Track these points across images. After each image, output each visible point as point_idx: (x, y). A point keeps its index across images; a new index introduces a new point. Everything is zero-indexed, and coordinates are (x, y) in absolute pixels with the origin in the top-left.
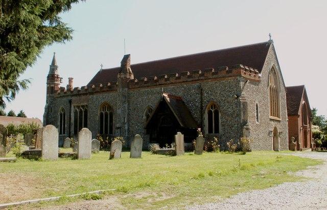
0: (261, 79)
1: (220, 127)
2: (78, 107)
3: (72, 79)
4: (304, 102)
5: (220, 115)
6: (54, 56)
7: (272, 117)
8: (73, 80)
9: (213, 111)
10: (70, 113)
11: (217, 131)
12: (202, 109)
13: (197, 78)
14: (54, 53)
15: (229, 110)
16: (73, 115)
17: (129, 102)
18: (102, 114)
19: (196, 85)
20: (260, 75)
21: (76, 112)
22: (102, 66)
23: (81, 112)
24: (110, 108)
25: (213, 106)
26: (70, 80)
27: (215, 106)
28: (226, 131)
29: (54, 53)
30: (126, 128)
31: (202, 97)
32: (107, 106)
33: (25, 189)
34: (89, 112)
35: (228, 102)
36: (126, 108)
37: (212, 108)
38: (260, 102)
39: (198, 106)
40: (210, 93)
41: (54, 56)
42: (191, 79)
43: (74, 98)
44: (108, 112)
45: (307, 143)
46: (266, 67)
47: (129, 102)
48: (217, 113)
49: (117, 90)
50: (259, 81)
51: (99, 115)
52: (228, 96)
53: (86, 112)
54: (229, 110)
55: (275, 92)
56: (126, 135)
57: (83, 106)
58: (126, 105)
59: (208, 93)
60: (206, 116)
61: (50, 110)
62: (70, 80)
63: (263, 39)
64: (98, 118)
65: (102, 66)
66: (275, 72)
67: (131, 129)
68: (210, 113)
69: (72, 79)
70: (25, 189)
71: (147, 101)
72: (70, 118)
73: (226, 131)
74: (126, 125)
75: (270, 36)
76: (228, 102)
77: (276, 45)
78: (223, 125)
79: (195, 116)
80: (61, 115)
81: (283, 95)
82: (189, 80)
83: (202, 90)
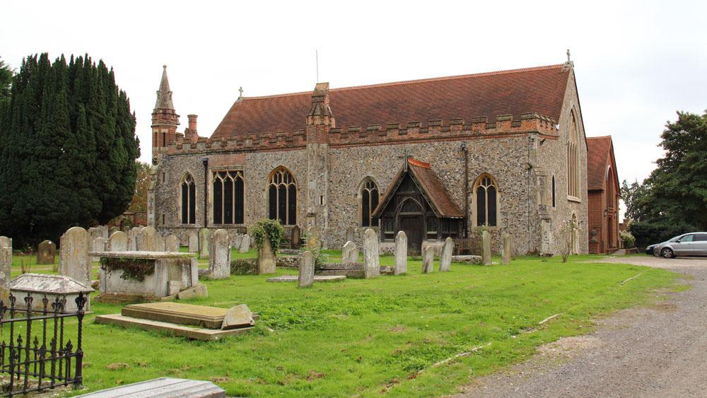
0: (559, 133)
1: (499, 217)
2: (223, 174)
3: (195, 116)
4: (609, 166)
5: (498, 196)
6: (165, 73)
7: (570, 198)
8: (198, 120)
9: (486, 188)
10: (206, 183)
11: (493, 222)
12: (467, 185)
13: (458, 133)
14: (165, 67)
15: (515, 188)
16: (211, 188)
17: (330, 169)
18: (272, 189)
19: (457, 144)
20: (558, 127)
21: (217, 184)
22: (241, 90)
23: (228, 182)
24: (289, 177)
25: (486, 179)
26: (192, 119)
27: (489, 180)
28: (510, 223)
29: (165, 67)
30: (326, 215)
31: (467, 167)
32: (281, 174)
33: (587, 339)
34: (247, 185)
35: (513, 175)
36: (326, 180)
37: (484, 184)
38: (556, 173)
39: (459, 181)
40: (480, 157)
41: (165, 73)
42: (448, 134)
43: (211, 158)
44: (287, 186)
45: (612, 233)
46: (565, 113)
47: (330, 169)
48: (492, 192)
49: (304, 147)
50: (556, 137)
51: (267, 190)
52: (514, 165)
53: (240, 183)
54: (515, 188)
55: (572, 150)
56: (326, 228)
57: (233, 173)
58: (325, 174)
59: (477, 159)
60: (474, 197)
61: (161, 178)
62: (192, 119)
63: (557, 59)
64: (265, 196)
65: (241, 90)
66: (576, 116)
67: (334, 217)
68: (480, 192)
69: (195, 116)
70: (587, 339)
71: (365, 167)
72: (206, 195)
73: (510, 223)
74: (325, 210)
75: (568, 54)
76: (513, 175)
77: (577, 70)
78: (504, 213)
79: (455, 196)
80: (185, 187)
81: (582, 154)
82: (444, 135)
83: (466, 152)
